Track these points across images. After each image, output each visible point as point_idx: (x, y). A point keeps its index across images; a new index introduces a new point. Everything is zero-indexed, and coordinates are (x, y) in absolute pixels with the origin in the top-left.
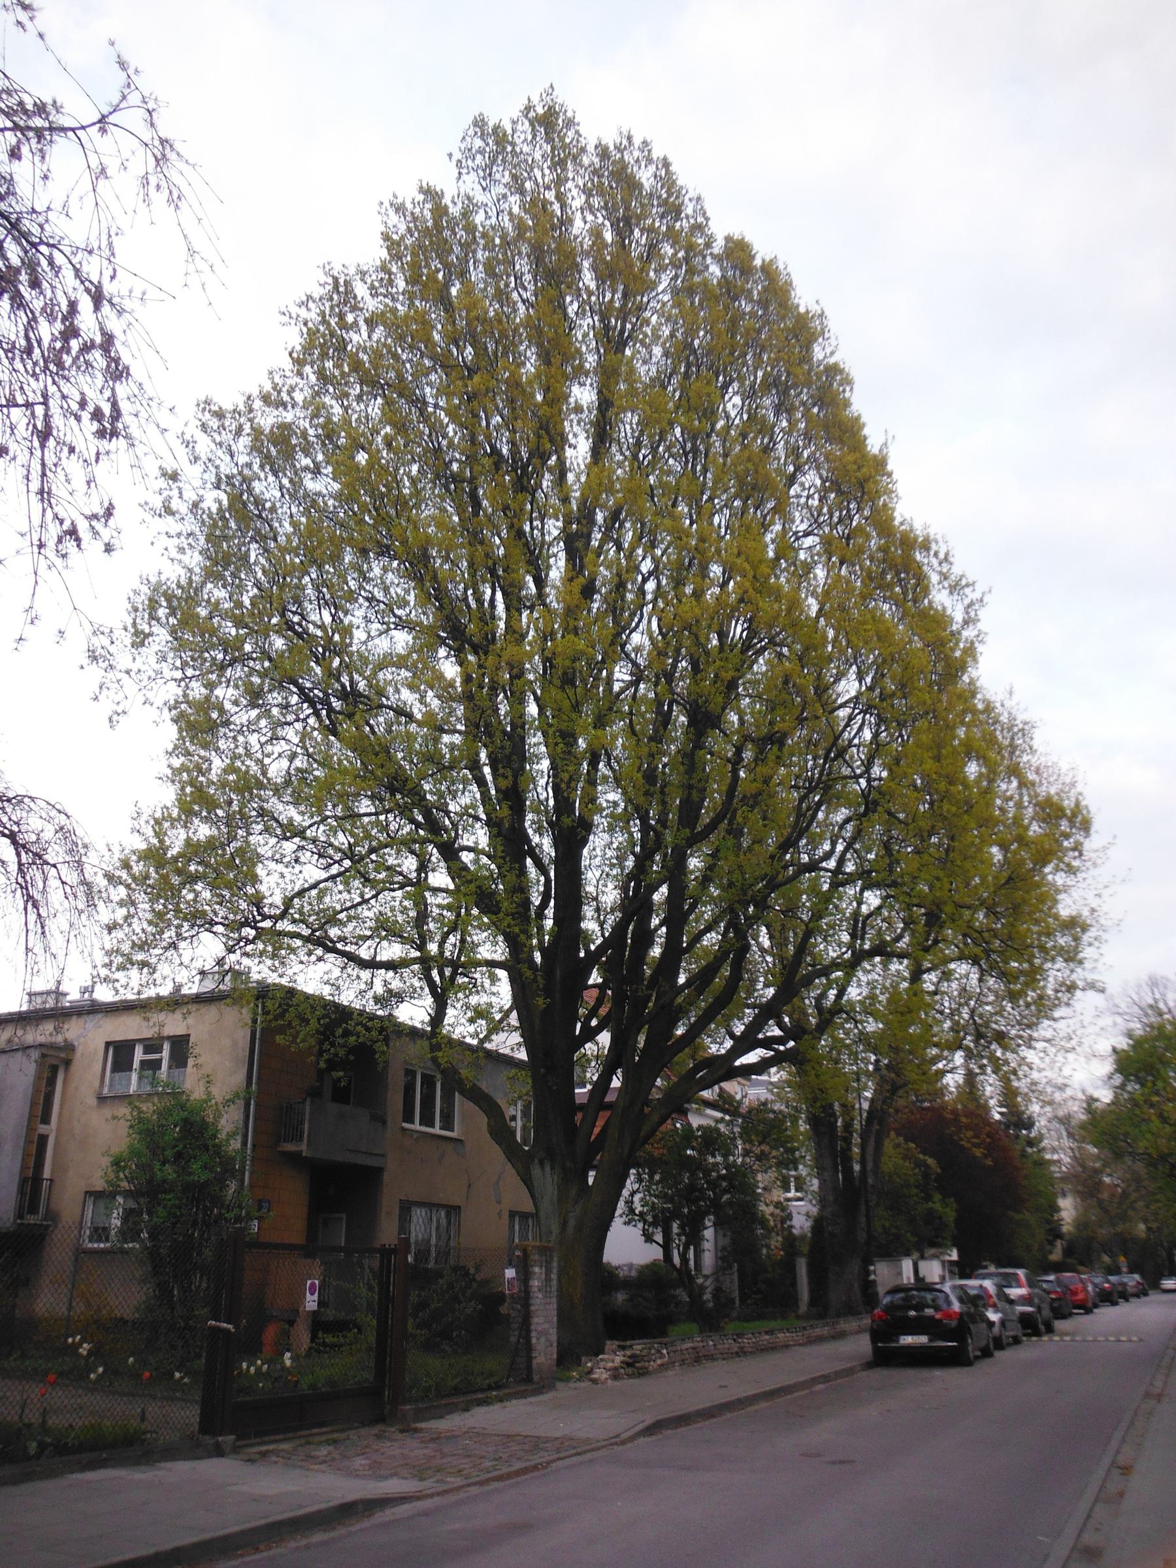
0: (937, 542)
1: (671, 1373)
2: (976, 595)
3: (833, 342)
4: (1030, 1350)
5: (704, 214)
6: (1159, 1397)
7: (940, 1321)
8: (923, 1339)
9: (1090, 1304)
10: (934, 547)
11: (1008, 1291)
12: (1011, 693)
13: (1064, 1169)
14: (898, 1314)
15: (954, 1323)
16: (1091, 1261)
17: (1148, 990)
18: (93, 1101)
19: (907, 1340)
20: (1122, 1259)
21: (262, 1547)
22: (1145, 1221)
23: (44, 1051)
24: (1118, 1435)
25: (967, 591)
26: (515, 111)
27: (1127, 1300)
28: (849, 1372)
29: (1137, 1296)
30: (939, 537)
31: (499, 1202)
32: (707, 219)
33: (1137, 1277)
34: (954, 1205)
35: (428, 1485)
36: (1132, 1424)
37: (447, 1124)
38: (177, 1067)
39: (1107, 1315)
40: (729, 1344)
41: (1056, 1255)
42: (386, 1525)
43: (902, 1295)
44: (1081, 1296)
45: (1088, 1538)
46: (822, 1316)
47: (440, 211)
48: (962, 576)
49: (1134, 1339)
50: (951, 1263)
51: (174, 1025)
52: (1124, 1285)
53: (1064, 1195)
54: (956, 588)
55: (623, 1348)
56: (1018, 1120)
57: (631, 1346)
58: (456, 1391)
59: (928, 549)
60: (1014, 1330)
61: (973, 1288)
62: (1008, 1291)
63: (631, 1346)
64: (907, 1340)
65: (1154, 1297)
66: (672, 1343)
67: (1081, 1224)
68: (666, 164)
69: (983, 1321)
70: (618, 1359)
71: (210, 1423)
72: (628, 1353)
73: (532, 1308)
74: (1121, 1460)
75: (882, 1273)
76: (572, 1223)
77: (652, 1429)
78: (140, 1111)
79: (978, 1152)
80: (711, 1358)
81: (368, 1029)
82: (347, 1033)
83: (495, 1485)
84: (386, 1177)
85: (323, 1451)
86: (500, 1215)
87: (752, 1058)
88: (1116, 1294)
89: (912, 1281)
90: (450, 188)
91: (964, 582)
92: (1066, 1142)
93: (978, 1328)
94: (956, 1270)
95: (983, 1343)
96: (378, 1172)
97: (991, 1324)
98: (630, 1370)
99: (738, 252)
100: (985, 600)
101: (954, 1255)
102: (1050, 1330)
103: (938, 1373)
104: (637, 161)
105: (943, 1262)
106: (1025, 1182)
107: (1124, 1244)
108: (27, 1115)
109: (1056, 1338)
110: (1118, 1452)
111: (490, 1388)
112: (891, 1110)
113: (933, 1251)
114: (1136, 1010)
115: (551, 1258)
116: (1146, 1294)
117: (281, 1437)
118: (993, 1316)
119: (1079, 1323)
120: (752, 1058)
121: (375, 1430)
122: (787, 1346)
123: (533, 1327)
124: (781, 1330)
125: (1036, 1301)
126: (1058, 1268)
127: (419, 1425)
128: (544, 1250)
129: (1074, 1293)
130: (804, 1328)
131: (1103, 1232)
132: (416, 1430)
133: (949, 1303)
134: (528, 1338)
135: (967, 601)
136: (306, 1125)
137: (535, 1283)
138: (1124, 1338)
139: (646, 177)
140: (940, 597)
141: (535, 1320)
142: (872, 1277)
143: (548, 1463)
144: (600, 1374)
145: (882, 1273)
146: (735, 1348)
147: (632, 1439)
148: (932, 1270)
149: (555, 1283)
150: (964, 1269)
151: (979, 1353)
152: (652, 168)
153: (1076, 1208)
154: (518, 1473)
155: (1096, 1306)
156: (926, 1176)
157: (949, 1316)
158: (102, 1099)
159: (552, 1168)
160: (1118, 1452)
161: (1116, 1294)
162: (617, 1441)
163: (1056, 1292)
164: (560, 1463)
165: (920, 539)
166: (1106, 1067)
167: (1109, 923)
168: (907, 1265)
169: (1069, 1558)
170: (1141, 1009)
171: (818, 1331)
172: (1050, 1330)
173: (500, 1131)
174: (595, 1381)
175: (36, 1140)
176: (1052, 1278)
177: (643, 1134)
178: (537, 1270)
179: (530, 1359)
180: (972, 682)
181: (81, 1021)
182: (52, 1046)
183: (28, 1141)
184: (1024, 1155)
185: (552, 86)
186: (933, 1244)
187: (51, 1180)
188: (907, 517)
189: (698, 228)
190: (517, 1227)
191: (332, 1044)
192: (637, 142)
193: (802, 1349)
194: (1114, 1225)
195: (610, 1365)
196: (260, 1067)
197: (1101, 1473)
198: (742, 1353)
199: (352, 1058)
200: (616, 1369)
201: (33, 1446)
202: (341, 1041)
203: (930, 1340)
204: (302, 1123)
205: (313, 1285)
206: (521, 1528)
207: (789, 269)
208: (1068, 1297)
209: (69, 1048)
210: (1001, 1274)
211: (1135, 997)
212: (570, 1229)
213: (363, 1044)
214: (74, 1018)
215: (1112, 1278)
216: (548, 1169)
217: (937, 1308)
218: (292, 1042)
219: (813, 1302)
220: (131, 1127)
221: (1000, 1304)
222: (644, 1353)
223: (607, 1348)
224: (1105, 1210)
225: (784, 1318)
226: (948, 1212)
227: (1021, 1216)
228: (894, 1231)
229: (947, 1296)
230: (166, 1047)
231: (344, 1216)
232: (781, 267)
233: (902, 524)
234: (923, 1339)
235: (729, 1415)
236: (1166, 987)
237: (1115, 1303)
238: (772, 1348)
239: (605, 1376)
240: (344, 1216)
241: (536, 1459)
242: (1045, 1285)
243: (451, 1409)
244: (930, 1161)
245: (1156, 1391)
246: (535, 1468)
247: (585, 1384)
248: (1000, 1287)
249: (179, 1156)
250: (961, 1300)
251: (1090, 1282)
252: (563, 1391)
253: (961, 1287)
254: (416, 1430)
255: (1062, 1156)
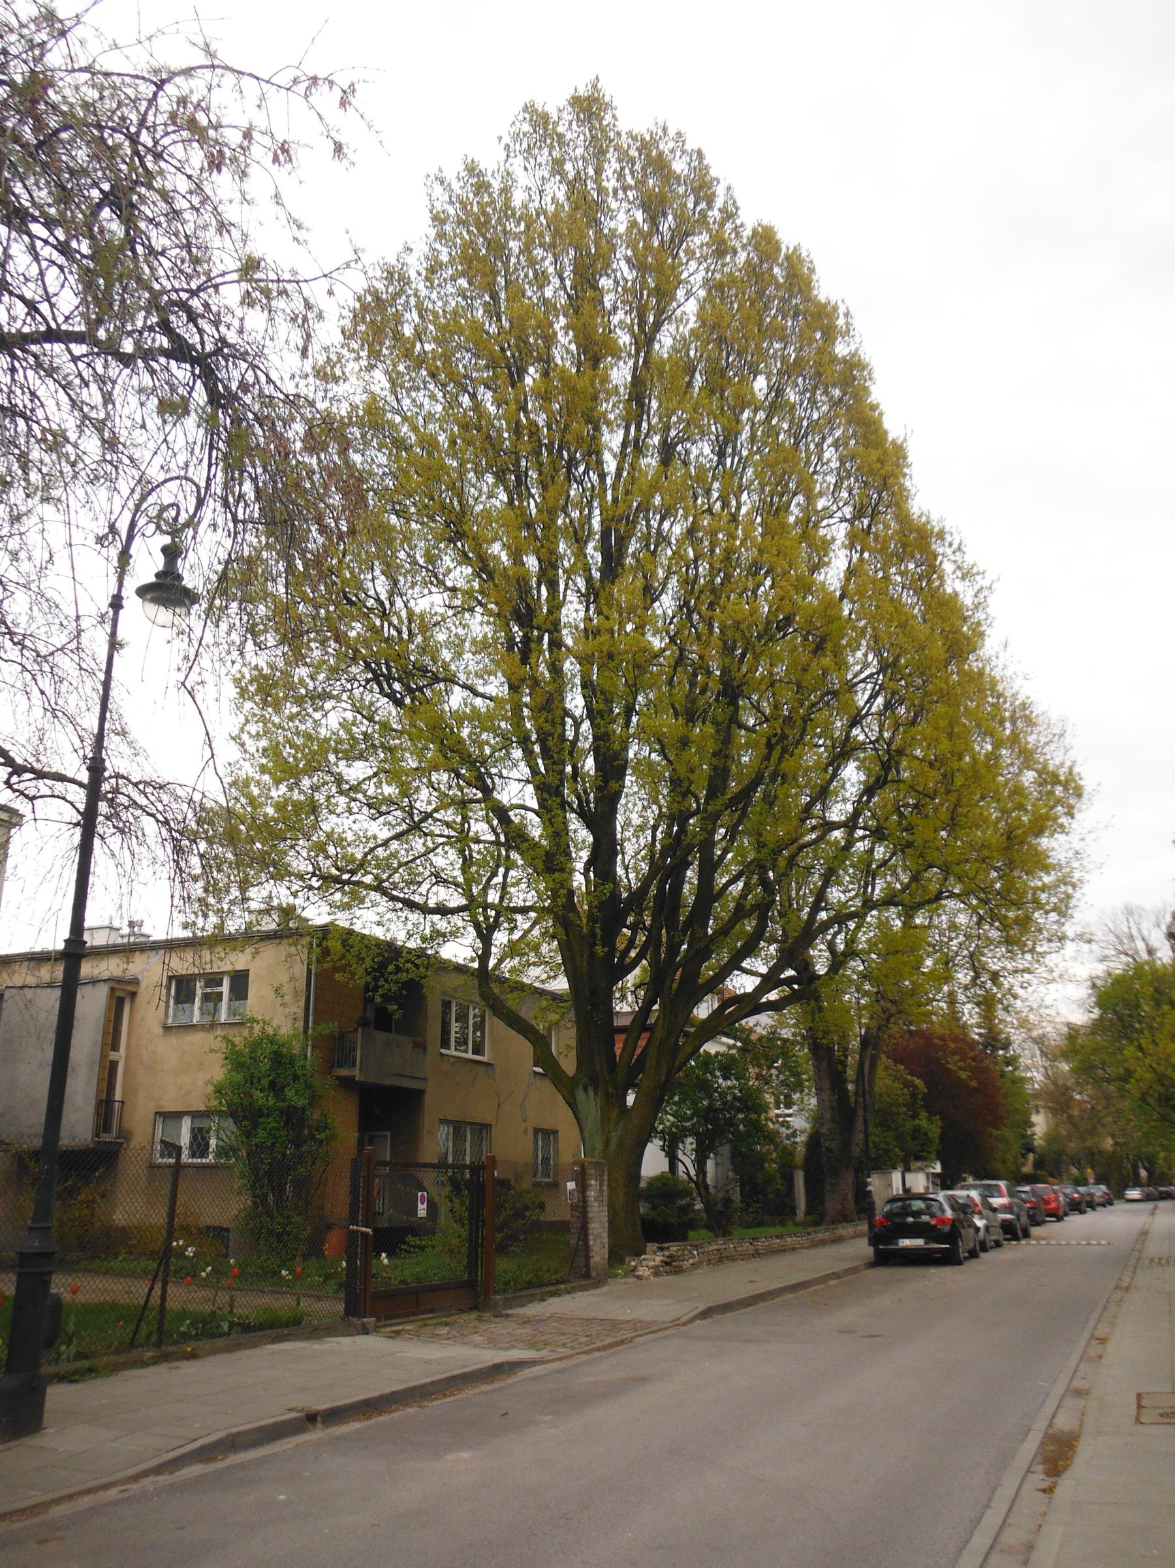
0: (951, 534)
1: (700, 1271)
2: (986, 583)
3: (857, 339)
4: (1011, 1252)
5: (735, 202)
6: (1127, 1289)
7: (935, 1226)
8: (919, 1242)
9: (1061, 1213)
10: (948, 538)
11: (991, 1200)
12: (1006, 646)
13: (1036, 1086)
14: (897, 1220)
15: (947, 1228)
16: (1060, 1175)
17: (1123, 919)
18: (159, 1031)
19: (906, 1243)
20: (1089, 1170)
21: (448, 1393)
22: (1113, 1136)
23: (114, 985)
24: (1095, 1315)
25: (978, 578)
26: (563, 102)
27: (1094, 1209)
28: (855, 1270)
29: (1104, 1206)
30: (954, 530)
31: (525, 1121)
32: (737, 209)
33: (1103, 1188)
34: (939, 1123)
35: (544, 1353)
36: (1105, 1309)
37: (478, 1050)
38: (237, 999)
39: (1075, 1222)
40: (826, 1236)
41: (1027, 1169)
42: (534, 1379)
43: (900, 1204)
44: (1053, 1205)
45: (1077, 1384)
46: (817, 1223)
47: (482, 187)
48: (974, 565)
49: (1103, 1242)
50: (935, 1175)
51: (239, 960)
52: (1091, 1195)
53: (1038, 1112)
54: (967, 575)
55: (662, 1249)
56: (995, 1040)
57: (668, 1248)
58: (530, 1285)
59: (943, 539)
60: (998, 1234)
61: (961, 1197)
62: (991, 1200)
63: (668, 1248)
64: (906, 1243)
65: (1119, 1206)
66: (701, 1246)
67: (1051, 1138)
68: (700, 154)
69: (970, 1226)
70: (659, 1259)
71: (354, 1308)
72: (667, 1253)
73: (590, 1215)
74: (1098, 1334)
75: (875, 1183)
76: (614, 1141)
77: (706, 1314)
78: (234, 1045)
79: (964, 1075)
80: (732, 1258)
81: (417, 966)
82: (398, 970)
83: (598, 1354)
84: (428, 1099)
85: (444, 1331)
86: (526, 1131)
87: (773, 996)
88: (1084, 1204)
89: (901, 1192)
90: (490, 161)
91: (975, 570)
92: (1039, 1060)
93: (967, 1233)
94: (938, 1181)
95: (971, 1245)
96: (421, 1093)
97: (977, 1229)
98: (668, 1268)
99: (765, 239)
100: (994, 587)
101: (938, 1168)
102: (1026, 1235)
103: (933, 1271)
104: (672, 151)
105: (927, 1175)
106: (1003, 1101)
107: (1092, 1157)
108: (100, 1043)
109: (1033, 1242)
110: (1095, 1328)
111: (558, 1282)
112: (886, 1036)
113: (919, 1164)
114: (1112, 938)
115: (603, 1171)
116: (1111, 1204)
117: (404, 1320)
118: (980, 1223)
119: (1051, 1229)
120: (773, 996)
121: (474, 1315)
122: (794, 1249)
123: (590, 1232)
124: (789, 1235)
125: (1016, 1209)
126: (1030, 1179)
127: (509, 1312)
128: (597, 1165)
129: (1048, 1202)
130: (809, 1234)
131: (1072, 1146)
132: (508, 1316)
133: (943, 1211)
134: (586, 1241)
135: (977, 587)
136: (359, 1052)
137: (592, 1194)
138: (1094, 1242)
139: (679, 166)
140: (952, 585)
141: (592, 1225)
142: (869, 1188)
143: (632, 1338)
144: (643, 1271)
145: (875, 1183)
146: (751, 1249)
147: (691, 1321)
148: (918, 1182)
149: (606, 1193)
150: (946, 1181)
151: (967, 1255)
152: (686, 159)
153: (1047, 1124)
154: (611, 1346)
155: (1066, 1214)
156: (914, 1095)
157: (942, 1221)
158: (167, 1029)
159: (596, 1093)
160: (1095, 1328)
161: (1084, 1204)
162: (677, 1323)
163: (1031, 1202)
164: (641, 1339)
165: (936, 530)
166: (1082, 992)
167: (1092, 866)
168: (896, 1176)
169: (1064, 1395)
170: (1117, 937)
171: (820, 1236)
172: (1026, 1235)
173: (544, 1057)
174: (639, 1277)
175: (108, 1065)
176: (1027, 1188)
177: (677, 1063)
178: (593, 1182)
179: (588, 1258)
180: (894, 442)
181: (144, 957)
182: (118, 981)
183: (102, 1067)
184: (1002, 1074)
185: (597, 78)
186: (918, 1158)
187: (123, 1102)
188: (925, 510)
189: (729, 215)
190: (540, 1143)
191: (386, 981)
192: (672, 132)
193: (806, 1251)
194: (1083, 1139)
195: (652, 1264)
196: (316, 999)
197: (1083, 1343)
198: (757, 1254)
199: (404, 992)
200: (657, 1267)
201: (225, 1326)
202: (394, 977)
203: (926, 1243)
204: (355, 1050)
205: (422, 1196)
206: (643, 1380)
207: (812, 257)
208: (1042, 1206)
209: (135, 981)
210: (984, 1186)
211: (1111, 925)
212: (613, 1147)
213: (412, 980)
214: (138, 953)
215: (1081, 1189)
216: (591, 1093)
217: (932, 1215)
218: (350, 979)
219: (810, 1210)
220: (226, 1058)
221: (985, 1212)
222: (679, 1253)
223: (648, 1249)
224: (1075, 1125)
225: (783, 1224)
226: (933, 1128)
227: (999, 1132)
228: (883, 1145)
229: (941, 1204)
230: (226, 982)
231: (389, 1133)
232: (804, 254)
233: (920, 517)
234: (919, 1242)
235: (763, 1304)
236: (1140, 916)
237: (1082, 1212)
238: (782, 1251)
239: (647, 1273)
240: (389, 1133)
241: (621, 1336)
242: (1023, 1196)
243: (531, 1299)
244: (918, 1082)
245: (1124, 1285)
246: (622, 1342)
247: (631, 1280)
248: (984, 1198)
249: (272, 1084)
250: (953, 1209)
251: (1061, 1192)
252: (615, 1286)
253: (952, 1196)
254: (508, 1316)
255: (1035, 1074)
